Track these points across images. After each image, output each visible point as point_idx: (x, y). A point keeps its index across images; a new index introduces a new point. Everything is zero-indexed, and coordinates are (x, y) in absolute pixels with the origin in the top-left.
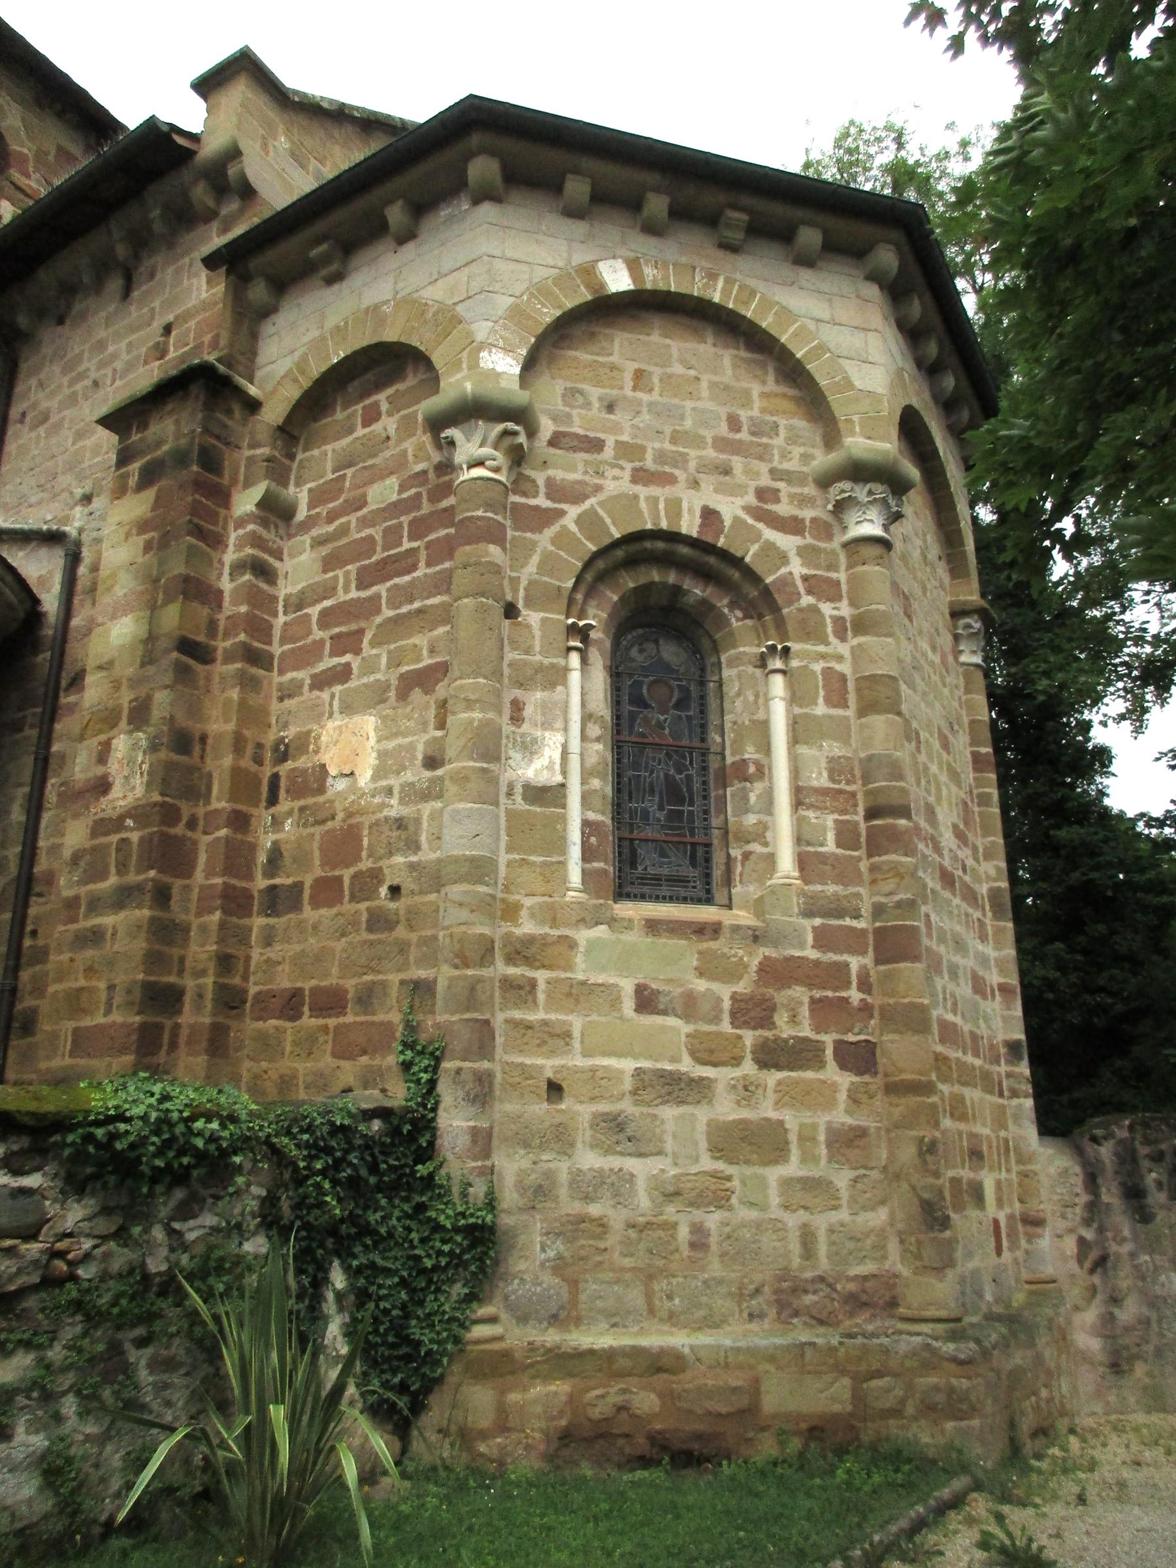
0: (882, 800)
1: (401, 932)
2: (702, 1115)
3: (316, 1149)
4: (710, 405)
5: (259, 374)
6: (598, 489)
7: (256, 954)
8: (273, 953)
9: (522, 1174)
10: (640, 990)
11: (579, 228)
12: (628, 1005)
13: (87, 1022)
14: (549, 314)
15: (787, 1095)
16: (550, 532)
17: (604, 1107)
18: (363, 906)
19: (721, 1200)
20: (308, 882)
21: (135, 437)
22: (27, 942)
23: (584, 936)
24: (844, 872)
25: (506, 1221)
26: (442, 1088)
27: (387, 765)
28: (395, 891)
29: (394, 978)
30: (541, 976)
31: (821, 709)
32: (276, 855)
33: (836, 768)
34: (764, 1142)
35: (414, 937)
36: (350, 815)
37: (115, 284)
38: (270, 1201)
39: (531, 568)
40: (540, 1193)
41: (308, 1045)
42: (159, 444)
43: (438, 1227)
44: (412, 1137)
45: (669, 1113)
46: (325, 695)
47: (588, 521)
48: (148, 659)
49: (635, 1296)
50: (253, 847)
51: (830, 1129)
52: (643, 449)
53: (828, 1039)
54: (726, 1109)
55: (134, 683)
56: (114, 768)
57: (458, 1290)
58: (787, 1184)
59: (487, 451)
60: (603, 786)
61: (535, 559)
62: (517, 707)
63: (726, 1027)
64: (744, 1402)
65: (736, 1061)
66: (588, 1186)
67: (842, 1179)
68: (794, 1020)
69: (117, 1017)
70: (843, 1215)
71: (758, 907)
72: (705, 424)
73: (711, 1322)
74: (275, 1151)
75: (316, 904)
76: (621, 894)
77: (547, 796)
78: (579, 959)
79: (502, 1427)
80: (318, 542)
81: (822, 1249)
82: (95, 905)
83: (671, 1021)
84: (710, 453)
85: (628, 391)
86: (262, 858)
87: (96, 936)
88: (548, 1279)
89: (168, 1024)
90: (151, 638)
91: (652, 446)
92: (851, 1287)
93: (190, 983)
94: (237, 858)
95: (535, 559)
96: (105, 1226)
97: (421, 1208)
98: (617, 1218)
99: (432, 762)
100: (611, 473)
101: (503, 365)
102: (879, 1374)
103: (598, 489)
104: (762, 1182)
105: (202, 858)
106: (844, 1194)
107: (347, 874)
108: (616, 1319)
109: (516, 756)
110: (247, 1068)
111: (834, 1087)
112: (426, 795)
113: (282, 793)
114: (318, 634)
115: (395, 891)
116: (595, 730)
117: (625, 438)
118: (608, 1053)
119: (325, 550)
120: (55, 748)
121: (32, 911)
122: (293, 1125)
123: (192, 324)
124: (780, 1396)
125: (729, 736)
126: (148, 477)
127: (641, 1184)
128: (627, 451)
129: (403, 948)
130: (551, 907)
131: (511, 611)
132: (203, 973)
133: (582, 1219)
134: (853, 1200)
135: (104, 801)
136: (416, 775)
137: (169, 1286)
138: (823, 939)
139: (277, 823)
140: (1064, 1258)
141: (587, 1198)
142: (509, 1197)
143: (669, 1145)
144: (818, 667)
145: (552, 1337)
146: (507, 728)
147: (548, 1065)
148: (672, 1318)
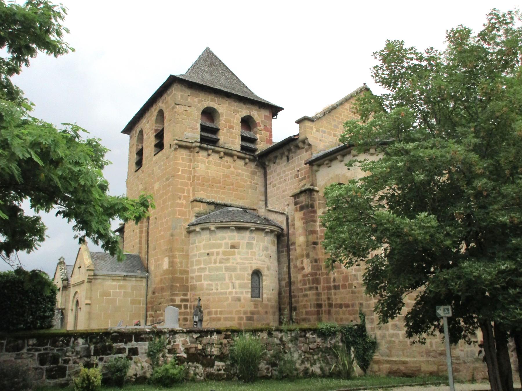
1: (357, 294)
3: (347, 331)
5: (318, 184)
7: (333, 296)
8: (337, 296)
9: (380, 334)
13: (307, 310)
18: (350, 289)
20: (341, 284)
21: (297, 200)
22: (292, 294)
25: (378, 341)
26: (366, 321)
28: (355, 287)
29: (357, 302)
32: (334, 280)
36: (346, 273)
37: (285, 158)
38: (342, 338)
40: (384, 337)
41: (344, 313)
42: (302, 202)
43: (367, 342)
44: (362, 328)
48: (307, 246)
49: (401, 353)
50: (330, 278)
55: (306, 250)
56: (305, 265)
57: (371, 351)
64: (418, 369)
66: (393, 335)
69: (313, 309)
73: (414, 357)
74: (341, 332)
75: (343, 288)
79: (379, 370)
81: (434, 346)
82: (305, 290)
86: (332, 280)
87: (306, 295)
88: (386, 350)
89: (321, 310)
90: (307, 241)
92: (440, 352)
93: (323, 303)
94: (328, 281)
96: (323, 341)
97: (364, 339)
98: (397, 341)
102: (443, 365)
105: (322, 281)
107: (347, 284)
108: (398, 356)
110: (334, 316)
115: (355, 287)
120: (291, 257)
121: (292, 288)
122: (344, 328)
123: (303, 171)
124: (425, 368)
126: (302, 208)
127: (401, 335)
129: (358, 297)
132: (325, 301)
133: (391, 341)
135: (304, 271)
137: (330, 348)
139: (334, 274)
141: (392, 337)
142: (378, 337)
145: (387, 359)
148: (407, 356)
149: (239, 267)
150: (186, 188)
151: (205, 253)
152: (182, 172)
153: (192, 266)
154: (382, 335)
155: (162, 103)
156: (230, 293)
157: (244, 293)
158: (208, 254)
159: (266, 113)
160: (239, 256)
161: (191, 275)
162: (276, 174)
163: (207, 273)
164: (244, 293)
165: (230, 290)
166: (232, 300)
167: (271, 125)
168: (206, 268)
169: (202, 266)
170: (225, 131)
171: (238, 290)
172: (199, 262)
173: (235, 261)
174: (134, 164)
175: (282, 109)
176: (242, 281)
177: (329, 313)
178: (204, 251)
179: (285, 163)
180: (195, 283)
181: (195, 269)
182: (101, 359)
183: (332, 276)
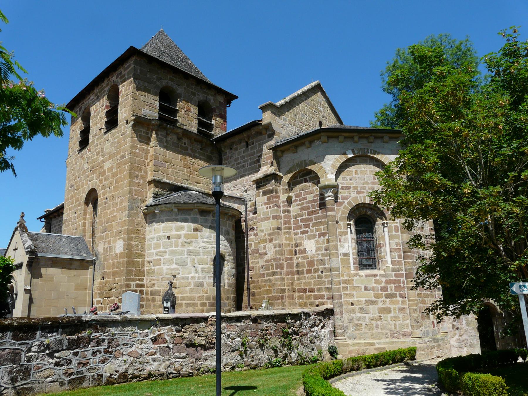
0: (405, 250)
1: (324, 279)
2: (376, 306)
4: (369, 175)
6: (350, 196)
10: (365, 287)
11: (342, 144)
12: (363, 289)
14: (338, 165)
15: (391, 303)
16: (343, 206)
17: (360, 306)
18: (316, 274)
19: (380, 320)
22: (250, 279)
23: (355, 278)
24: (399, 263)
27: (318, 249)
30: (348, 286)
31: (394, 233)
33: (397, 244)
34: (387, 310)
35: (326, 280)
39: (340, 213)
45: (371, 306)
46: (304, 235)
47: (349, 203)
50: (293, 263)
51: (398, 308)
52: (357, 187)
53: (398, 293)
54: (380, 305)
58: (391, 317)
59: (331, 194)
60: (355, 251)
61: (341, 212)
62: (340, 239)
63: (380, 292)
65: (382, 297)
66: (359, 319)
67: (401, 316)
68: (391, 290)
70: (401, 321)
71: (384, 270)
72: (369, 180)
75: (307, 273)
76: (360, 269)
77: (346, 255)
78: (354, 282)
80: (298, 205)
81: (398, 327)
83: (370, 292)
84: (370, 185)
85: (354, 176)
86: (295, 265)
91: (359, 186)
94: (290, 266)
95: (341, 212)
99: (326, 250)
100: (352, 193)
101: (332, 176)
103: (350, 196)
104: (387, 317)
105: (285, 266)
106: (401, 318)
107: (312, 269)
109: (341, 248)
111: (399, 301)
112: (326, 256)
113: (297, 253)
114: (300, 224)
116: (353, 241)
117: (354, 185)
118: (360, 298)
119: (300, 207)
125: (377, 239)
127: (367, 318)
128: (355, 188)
130: (349, 274)
131: (337, 222)
134: (403, 319)
136: (324, 252)
138: (396, 276)
140: (449, 328)
141: (359, 321)
143: (371, 312)
144: (393, 225)
146: (339, 244)
147: (351, 300)
149: (201, 251)
150: (144, 167)
151: (165, 236)
152: (140, 150)
153: (149, 249)
154: (350, 318)
155: (117, 77)
156: (193, 278)
157: (207, 278)
158: (169, 238)
159: (221, 99)
160: (203, 240)
161: (147, 259)
162: (233, 159)
163: (167, 256)
164: (207, 278)
165: (193, 275)
166: (195, 286)
167: (225, 112)
168: (166, 252)
169: (162, 249)
170: (183, 113)
171: (200, 275)
172: (157, 246)
173: (197, 245)
174: (78, 143)
175: (237, 97)
176: (204, 266)
177: (292, 297)
178: (164, 234)
179: (244, 149)
180: (153, 268)
181: (153, 253)
182: (76, 354)
183: (295, 262)
